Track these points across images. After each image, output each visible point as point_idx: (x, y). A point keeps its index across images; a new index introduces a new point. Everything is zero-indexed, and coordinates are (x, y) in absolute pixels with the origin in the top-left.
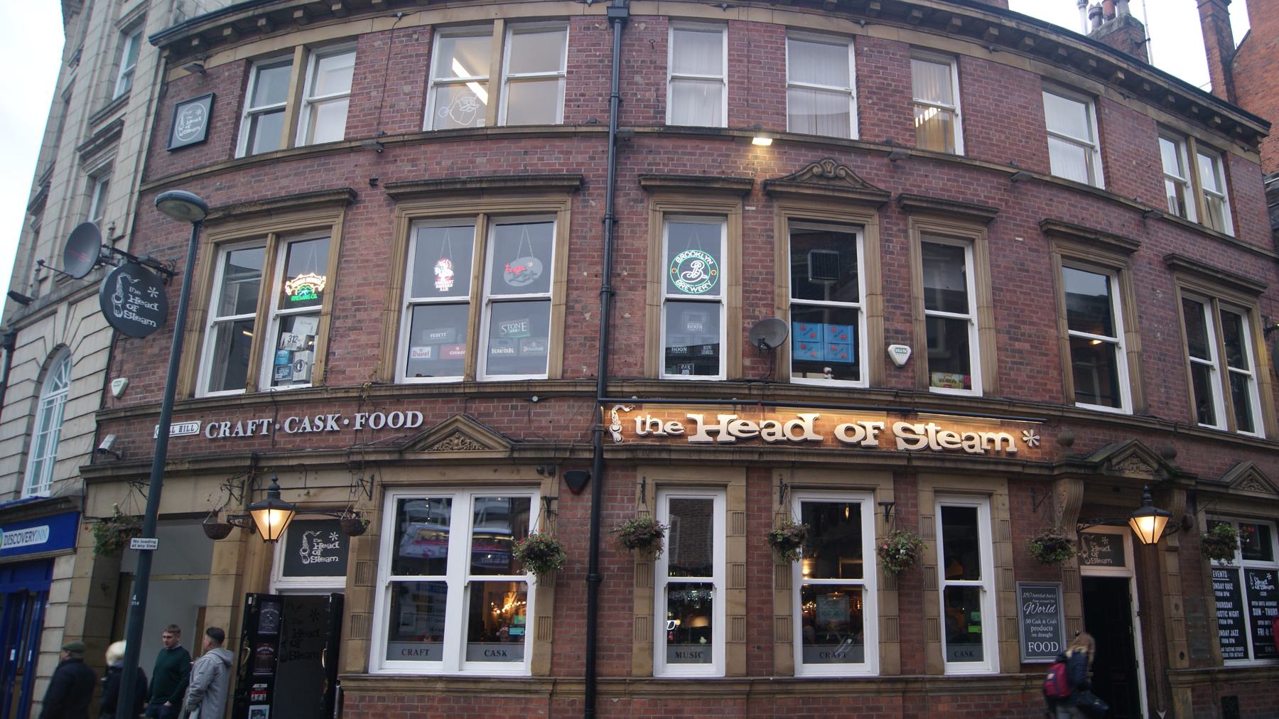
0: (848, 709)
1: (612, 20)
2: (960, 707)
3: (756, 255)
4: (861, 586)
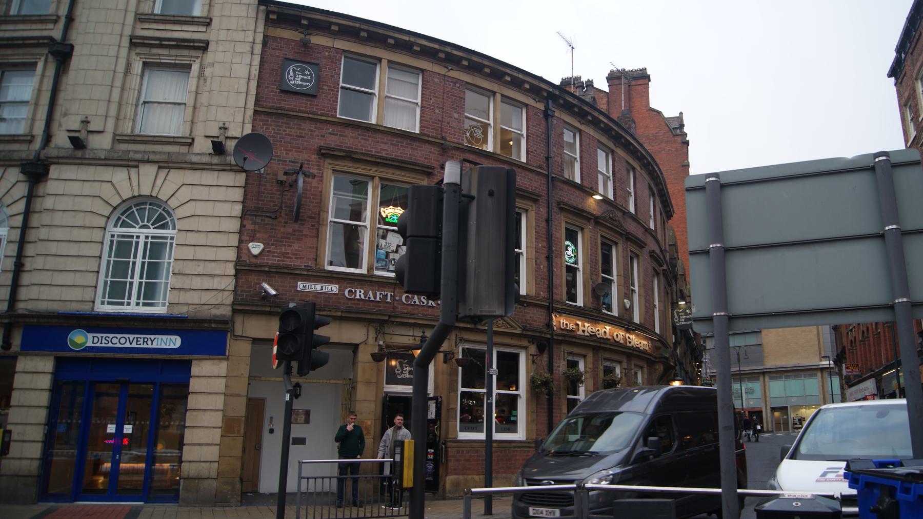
4: (517, 395)
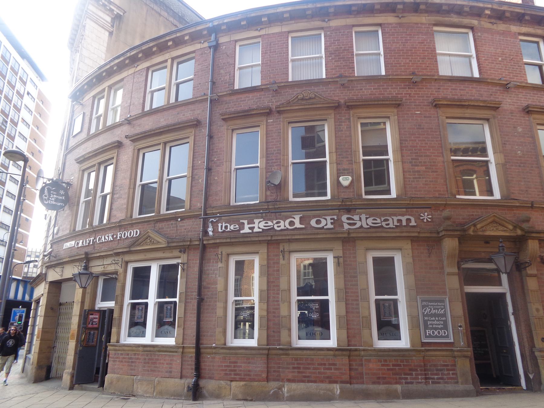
0: (318, 364)
1: (210, 47)
2: (383, 365)
3: (273, 142)
